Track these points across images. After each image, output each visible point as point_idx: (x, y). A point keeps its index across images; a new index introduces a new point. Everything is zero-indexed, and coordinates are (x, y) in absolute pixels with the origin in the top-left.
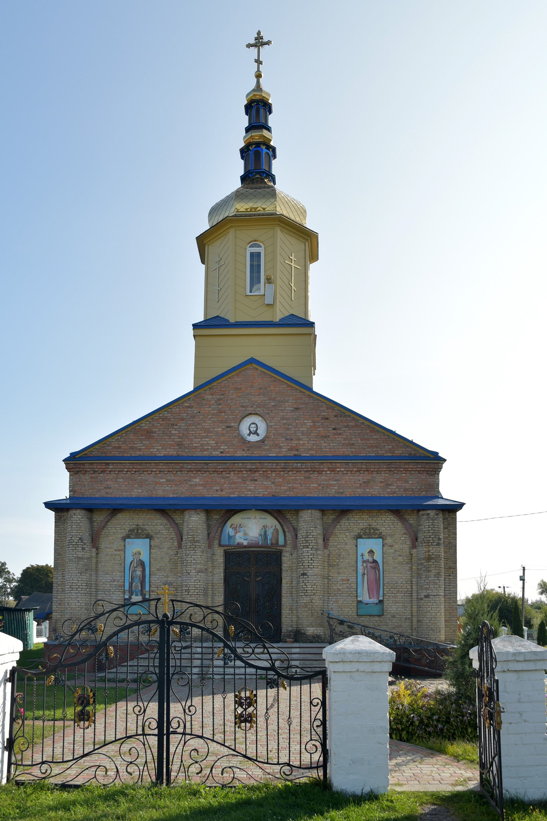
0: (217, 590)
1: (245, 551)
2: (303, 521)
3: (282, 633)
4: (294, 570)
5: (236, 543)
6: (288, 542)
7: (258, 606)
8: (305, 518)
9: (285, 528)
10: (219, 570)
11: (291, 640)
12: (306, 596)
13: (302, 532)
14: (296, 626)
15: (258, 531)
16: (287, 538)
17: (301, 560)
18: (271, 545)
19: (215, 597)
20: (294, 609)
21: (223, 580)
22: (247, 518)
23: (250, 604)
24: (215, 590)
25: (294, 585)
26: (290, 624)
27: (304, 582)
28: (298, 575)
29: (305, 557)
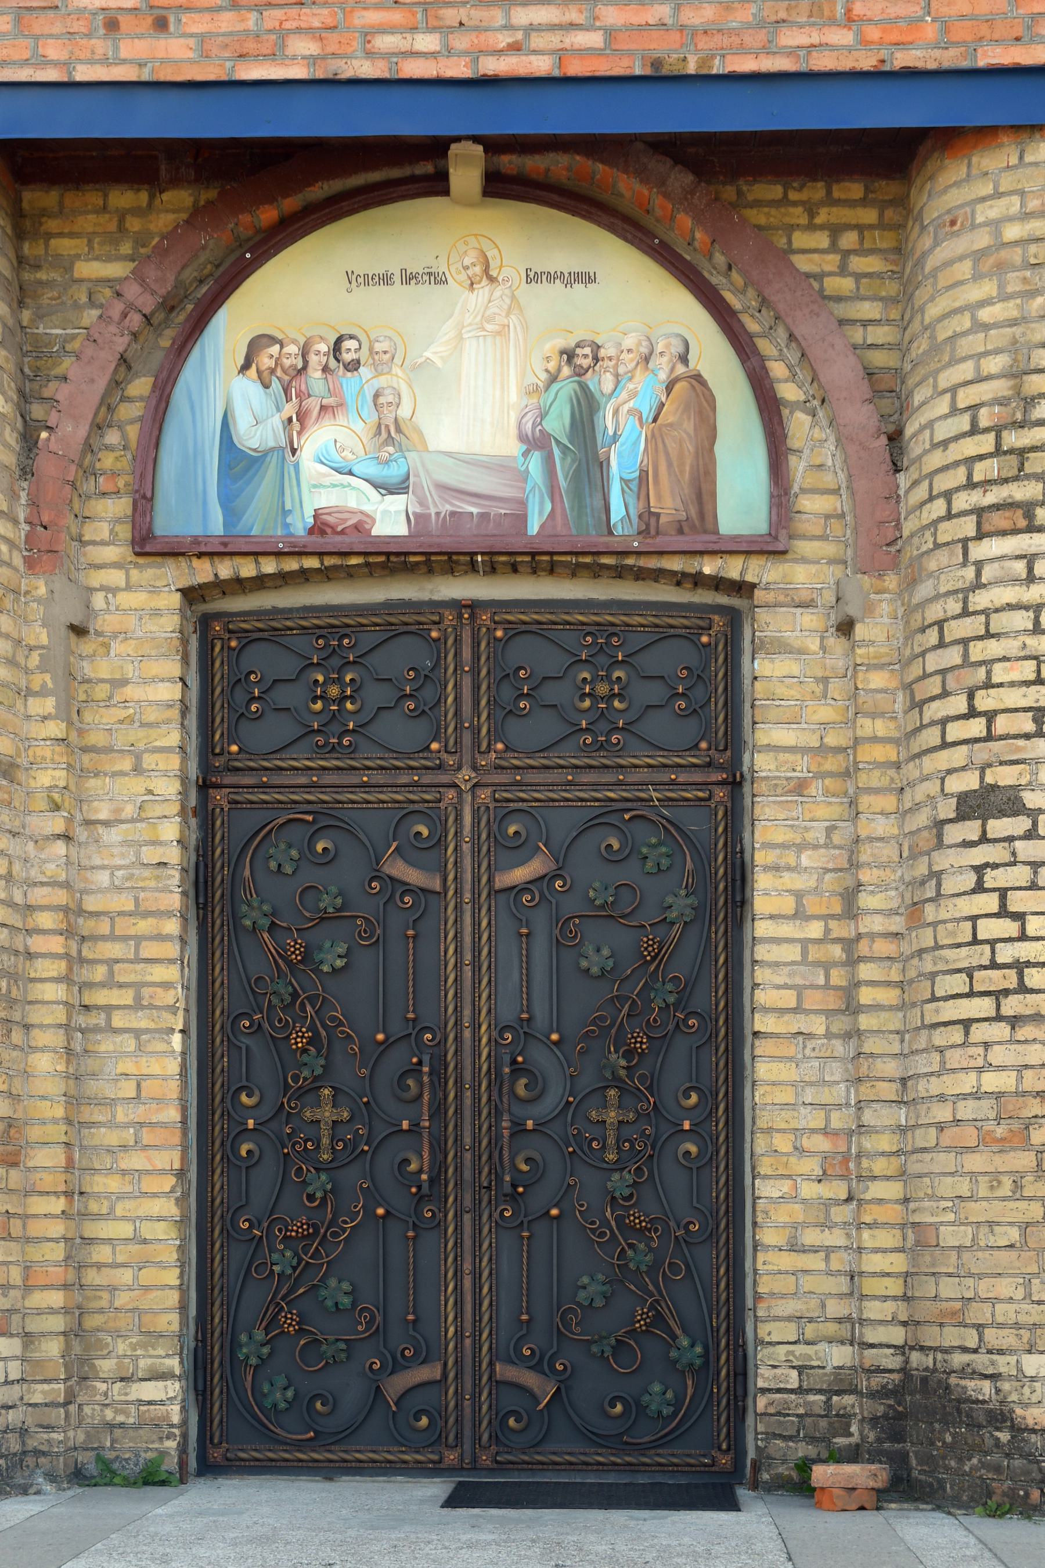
0: (125, 974)
1: (390, 606)
2: (978, 256)
3: (762, 1402)
4: (874, 779)
5: (300, 524)
6: (812, 505)
7: (518, 1130)
8: (996, 225)
9: (777, 369)
10: (136, 785)
11: (858, 1474)
12: (1014, 1021)
13: (965, 371)
14: (897, 1335)
15: (513, 396)
16: (798, 468)
17: (953, 656)
18: (644, 532)
19: (106, 1044)
20: (880, 1166)
21: (174, 877)
22: (409, 278)
23: (438, 1110)
24: (100, 973)
25: (876, 924)
26: (835, 1308)
27: (991, 879)
28: (922, 819)
29: (999, 623)
